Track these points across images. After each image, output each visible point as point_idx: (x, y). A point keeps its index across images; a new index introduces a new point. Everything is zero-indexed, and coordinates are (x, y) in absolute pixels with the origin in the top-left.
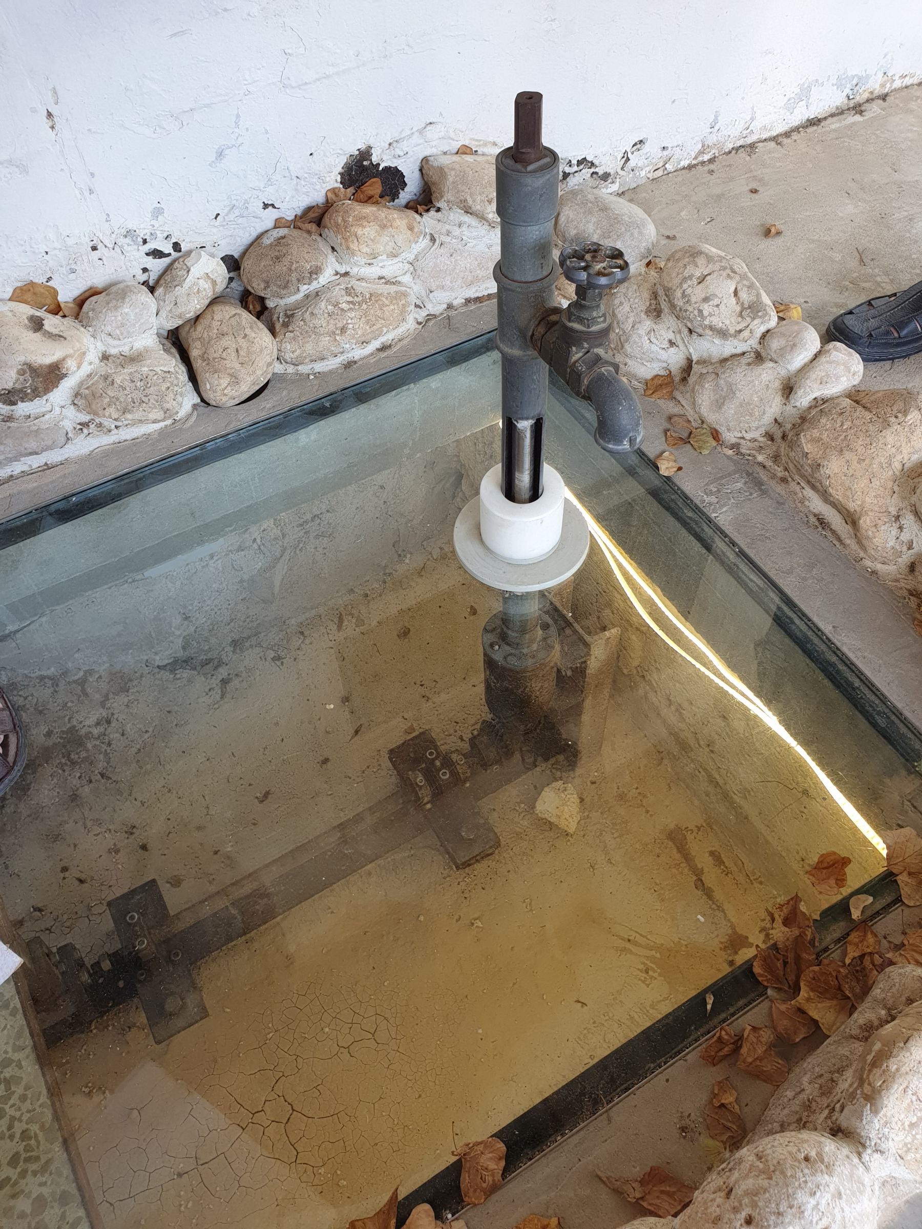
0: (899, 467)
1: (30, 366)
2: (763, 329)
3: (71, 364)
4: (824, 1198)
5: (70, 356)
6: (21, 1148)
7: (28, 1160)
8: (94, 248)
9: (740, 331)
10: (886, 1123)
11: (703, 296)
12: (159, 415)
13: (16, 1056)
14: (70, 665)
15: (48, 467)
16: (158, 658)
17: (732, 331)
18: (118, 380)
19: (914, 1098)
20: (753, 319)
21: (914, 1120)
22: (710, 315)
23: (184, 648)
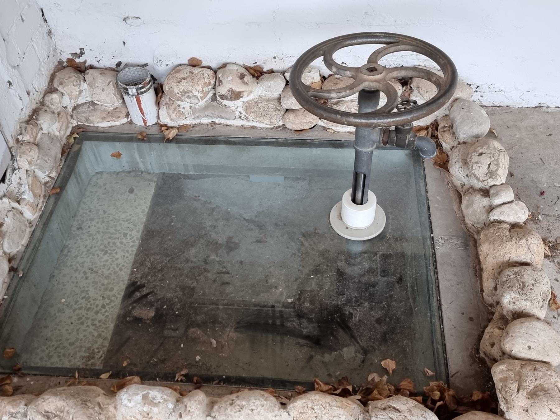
0: (507, 259)
1: (232, 90)
2: (492, 183)
3: (245, 94)
4: (257, 402)
5: (246, 91)
6: (104, 319)
7: (104, 323)
8: (274, 58)
9: (484, 181)
10: (294, 407)
11: (476, 161)
12: (269, 123)
13: (118, 296)
14: (213, 201)
15: (254, 128)
16: (245, 215)
17: (481, 179)
18: (259, 106)
19: (306, 406)
20: (490, 178)
21: (302, 411)
22: (475, 169)
23: (256, 216)
